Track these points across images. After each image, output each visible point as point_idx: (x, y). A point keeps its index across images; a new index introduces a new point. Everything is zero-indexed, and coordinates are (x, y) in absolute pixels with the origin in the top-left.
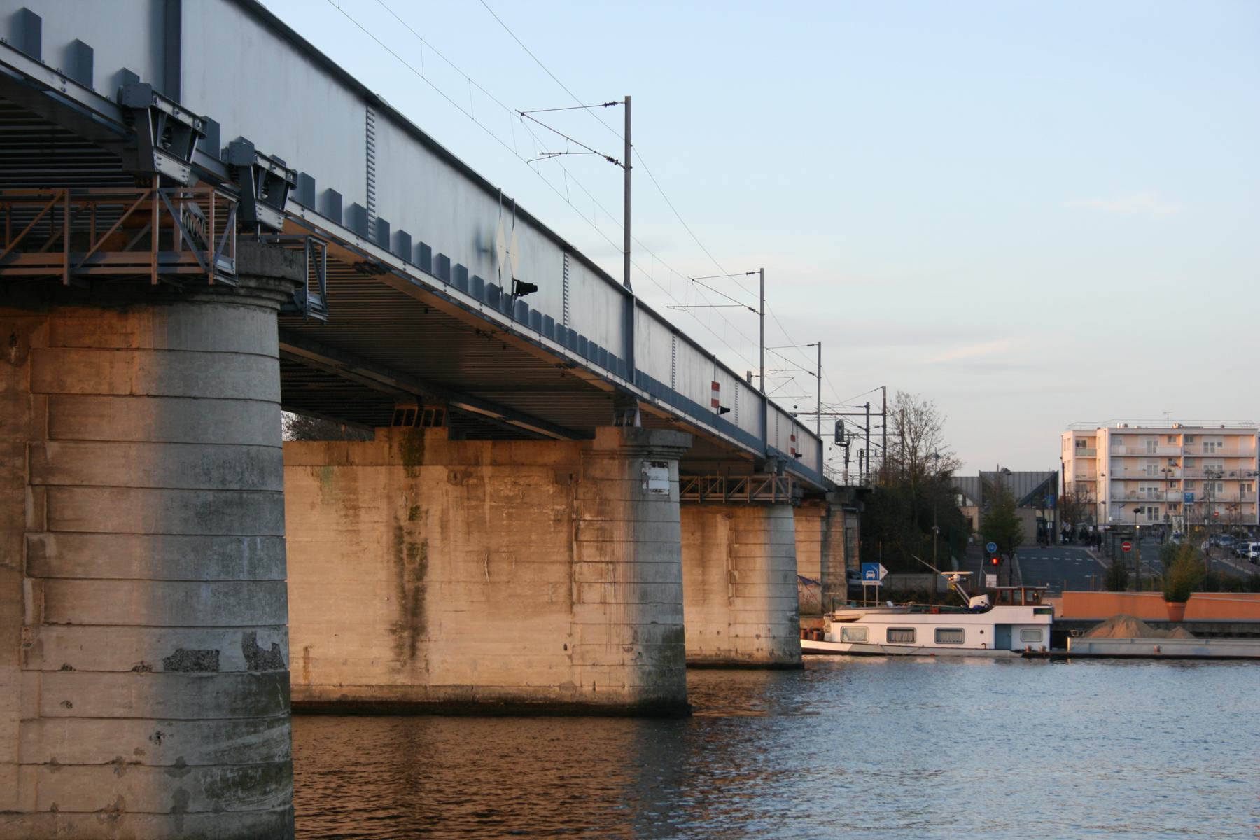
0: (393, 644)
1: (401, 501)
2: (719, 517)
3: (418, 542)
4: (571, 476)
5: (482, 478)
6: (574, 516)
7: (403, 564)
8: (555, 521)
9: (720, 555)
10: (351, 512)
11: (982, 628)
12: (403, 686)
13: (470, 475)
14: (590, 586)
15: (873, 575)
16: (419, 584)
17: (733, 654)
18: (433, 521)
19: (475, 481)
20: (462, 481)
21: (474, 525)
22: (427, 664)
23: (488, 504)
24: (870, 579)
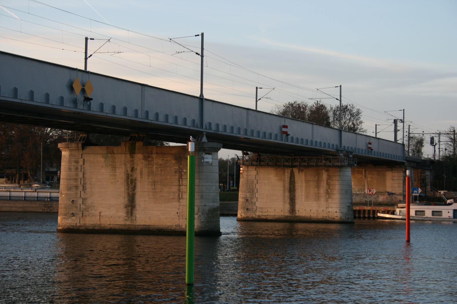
0: (125, 211)
1: (129, 165)
2: (324, 171)
3: (134, 178)
4: (180, 157)
5: (153, 158)
6: (181, 171)
7: (129, 186)
8: (175, 172)
9: (324, 184)
10: (114, 169)
11: (448, 211)
12: (129, 225)
13: (149, 157)
14: (185, 193)
15: (416, 192)
16: (134, 192)
17: (328, 218)
18: (138, 172)
19: (151, 159)
20: (147, 159)
21: (151, 173)
22: (136, 218)
23: (154, 166)
24: (415, 193)
